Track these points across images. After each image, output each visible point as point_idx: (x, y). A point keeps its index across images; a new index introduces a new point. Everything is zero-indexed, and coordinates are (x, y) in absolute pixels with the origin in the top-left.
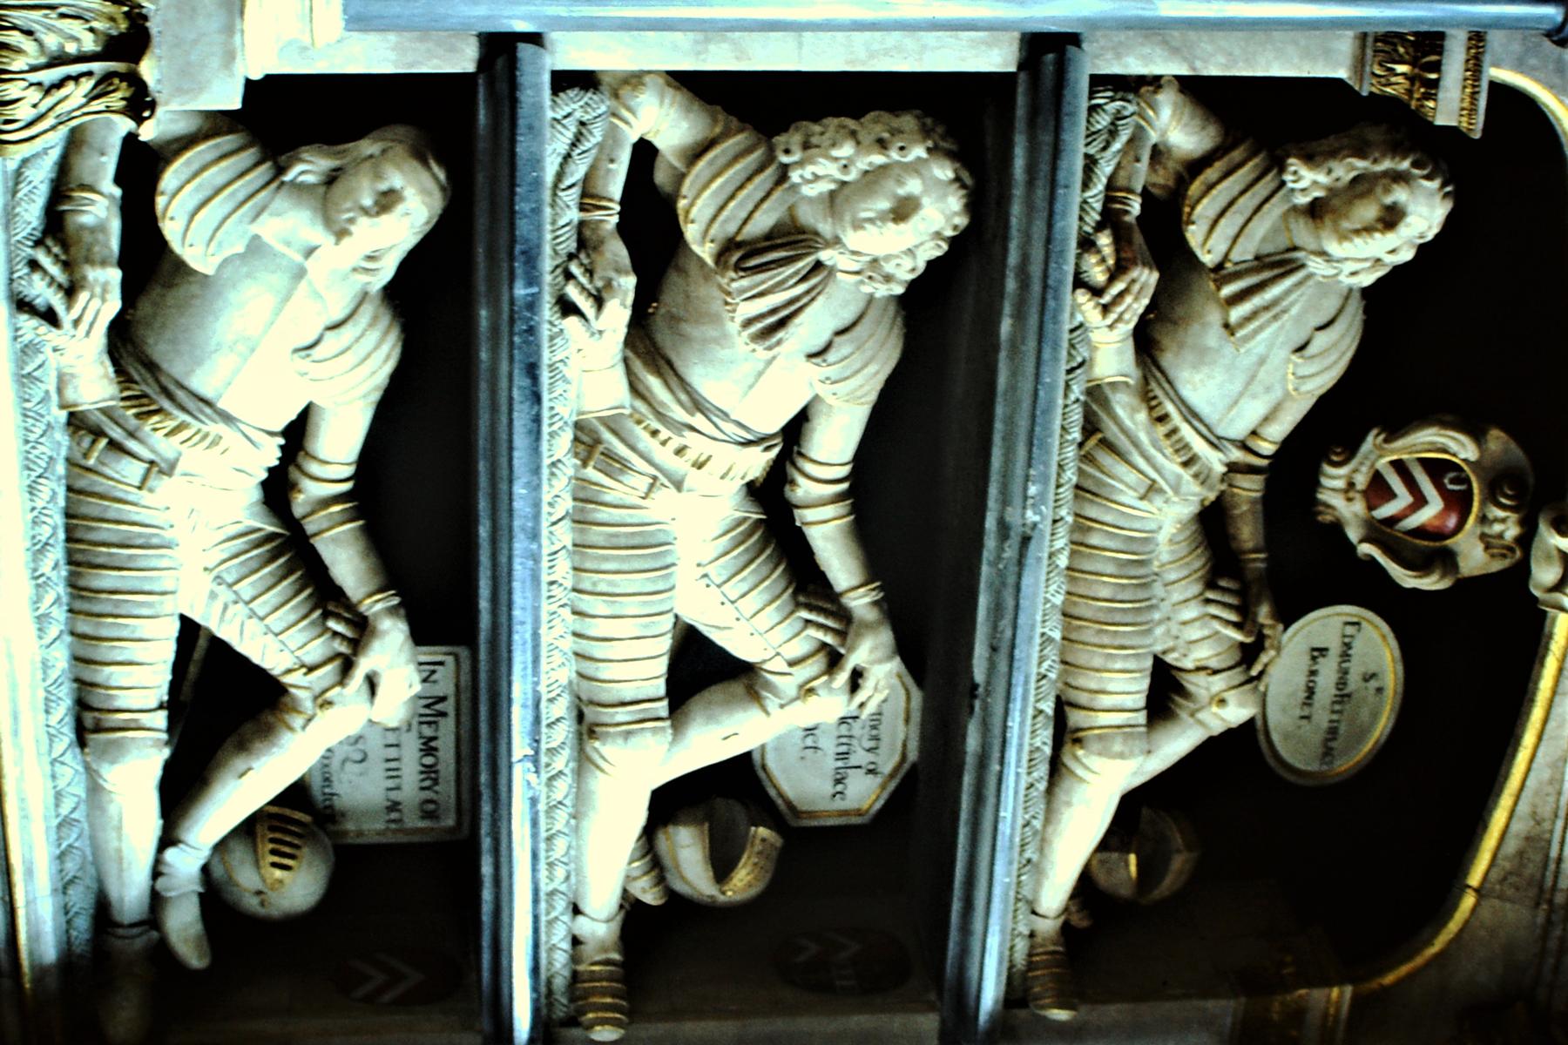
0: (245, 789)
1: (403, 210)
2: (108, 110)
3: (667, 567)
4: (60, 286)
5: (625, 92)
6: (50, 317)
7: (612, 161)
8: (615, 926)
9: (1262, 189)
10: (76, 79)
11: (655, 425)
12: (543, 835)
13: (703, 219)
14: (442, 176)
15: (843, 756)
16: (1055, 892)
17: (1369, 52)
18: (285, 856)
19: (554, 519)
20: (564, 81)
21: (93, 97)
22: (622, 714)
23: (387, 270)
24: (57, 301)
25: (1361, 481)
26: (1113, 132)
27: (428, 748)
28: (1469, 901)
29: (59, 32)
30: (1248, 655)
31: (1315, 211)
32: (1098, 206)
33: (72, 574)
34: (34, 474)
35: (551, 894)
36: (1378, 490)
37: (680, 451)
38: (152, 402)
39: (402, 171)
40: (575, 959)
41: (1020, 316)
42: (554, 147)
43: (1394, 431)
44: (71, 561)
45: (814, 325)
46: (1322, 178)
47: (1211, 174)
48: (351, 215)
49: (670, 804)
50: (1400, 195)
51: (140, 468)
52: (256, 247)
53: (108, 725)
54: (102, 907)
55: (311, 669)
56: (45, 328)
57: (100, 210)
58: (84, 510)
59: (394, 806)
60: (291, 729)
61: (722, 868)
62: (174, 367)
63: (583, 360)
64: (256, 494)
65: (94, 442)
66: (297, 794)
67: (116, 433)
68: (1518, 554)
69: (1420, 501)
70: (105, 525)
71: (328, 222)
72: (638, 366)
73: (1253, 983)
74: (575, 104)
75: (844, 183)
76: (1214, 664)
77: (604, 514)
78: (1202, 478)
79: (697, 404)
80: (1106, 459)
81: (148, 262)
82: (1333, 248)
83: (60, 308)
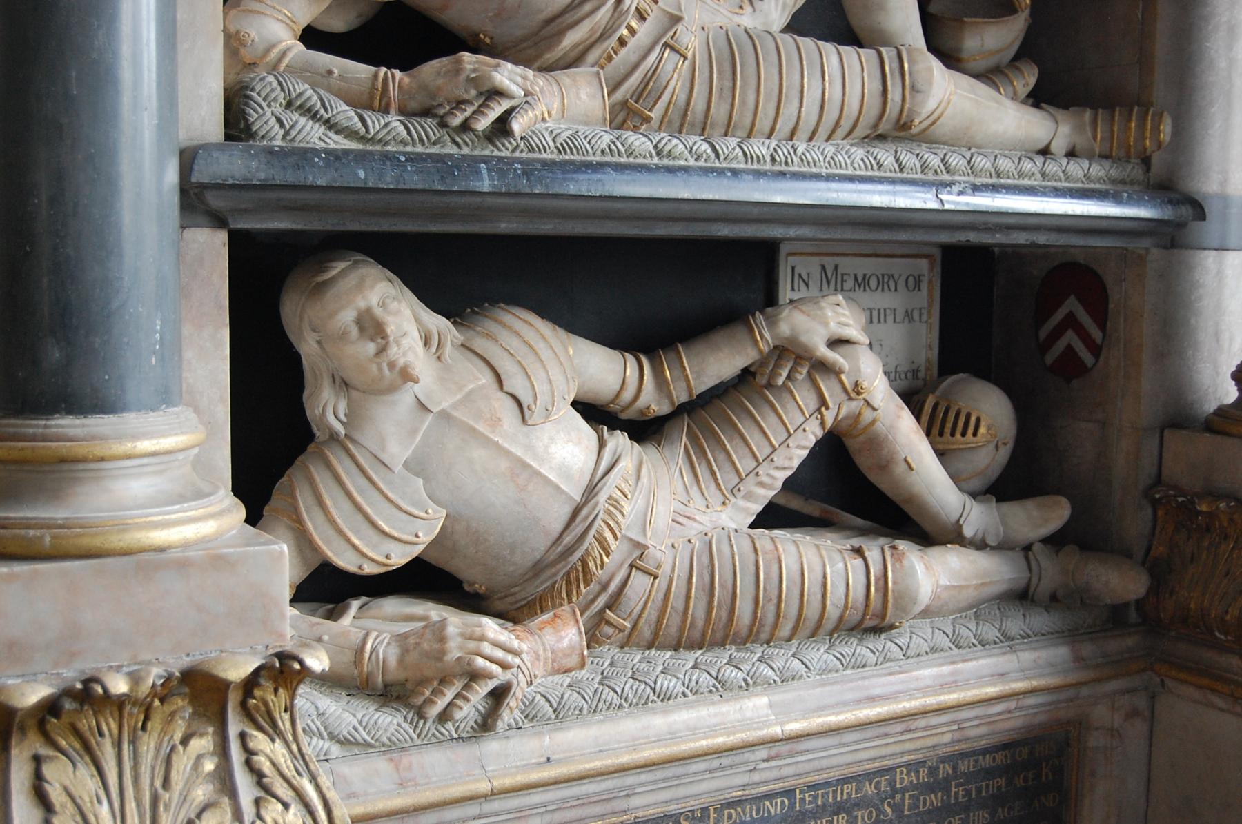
0: (918, 462)
1: (377, 318)
2: (290, 709)
3: (751, 37)
4: (467, 687)
5: (247, 55)
6: (499, 695)
7: (330, 72)
8: (1060, 114)
10: (249, 753)
11: (613, 41)
12: (994, 180)
14: (341, 265)
18: (969, 425)
19: (713, 156)
20: (237, 124)
21: (274, 731)
22: (894, 95)
23: (437, 323)
24: (482, 689)
29: (189, 785)
33: (734, 642)
34: (652, 696)
35: (1043, 174)
37: (642, 16)
38: (574, 568)
39: (336, 312)
40: (1091, 157)
42: (313, 135)
44: (722, 644)
48: (385, 366)
49: (951, 59)
52: (416, 466)
53: (879, 606)
54: (1021, 597)
55: (823, 403)
56: (511, 702)
58: (673, 630)
59: (908, 315)
60: (874, 421)
62: (538, 545)
65: (608, 623)
67: (602, 601)
70: (690, 612)
71: (392, 389)
74: (267, 118)
77: (698, 104)
81: (424, 579)
83: (491, 685)
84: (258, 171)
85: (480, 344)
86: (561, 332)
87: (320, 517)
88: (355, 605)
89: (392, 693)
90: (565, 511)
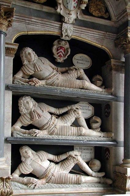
1: (28, 152)
6: (35, 185)
9: (27, 67)
13: (27, 122)
15: (87, 110)
16: (100, 89)
17: (10, 55)
18: (94, 164)
20: (12, 135)
21: (8, 183)
22: (79, 132)
25: (59, 58)
26: (19, 82)
27: (85, 149)
28: (103, 47)
30: (76, 69)
31: (29, 62)
32: (26, 83)
36: (60, 56)
40: (105, 137)
41: (37, 92)
42: (19, 136)
43: (53, 54)
45: (39, 111)
46: (25, 61)
47: (25, 72)
49: (90, 127)
50: (27, 53)
51: (53, 177)
57: (25, 179)
61: (97, 122)
62: (42, 173)
63: (41, 134)
64: (57, 165)
66: (88, 163)
67: (49, 179)
68: (66, 41)
69: (61, 52)
71: (28, 158)
72: (43, 129)
73: (111, 70)
74: (15, 135)
75: (25, 108)
76: (77, 73)
78: (57, 74)
79: (47, 123)
80: (54, 83)
81: (31, 175)
82: (33, 60)
83: (35, 184)
84: (13, 139)
85: (38, 154)
86: (47, 153)
87: (21, 169)
88: (25, 177)
89: (26, 184)
90: (45, 170)
